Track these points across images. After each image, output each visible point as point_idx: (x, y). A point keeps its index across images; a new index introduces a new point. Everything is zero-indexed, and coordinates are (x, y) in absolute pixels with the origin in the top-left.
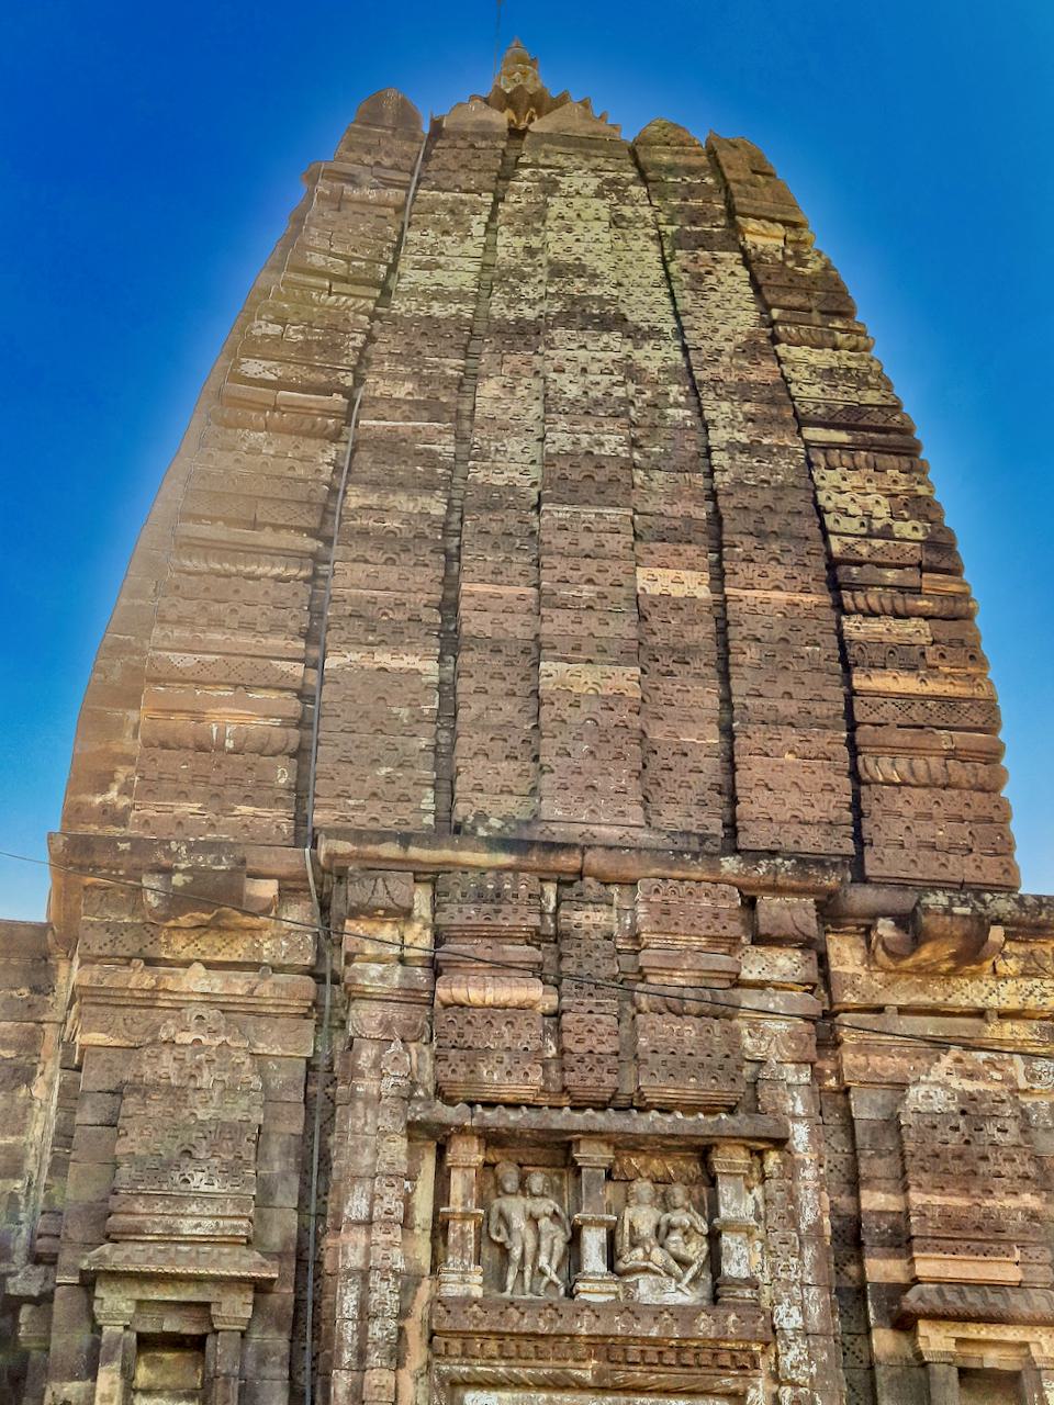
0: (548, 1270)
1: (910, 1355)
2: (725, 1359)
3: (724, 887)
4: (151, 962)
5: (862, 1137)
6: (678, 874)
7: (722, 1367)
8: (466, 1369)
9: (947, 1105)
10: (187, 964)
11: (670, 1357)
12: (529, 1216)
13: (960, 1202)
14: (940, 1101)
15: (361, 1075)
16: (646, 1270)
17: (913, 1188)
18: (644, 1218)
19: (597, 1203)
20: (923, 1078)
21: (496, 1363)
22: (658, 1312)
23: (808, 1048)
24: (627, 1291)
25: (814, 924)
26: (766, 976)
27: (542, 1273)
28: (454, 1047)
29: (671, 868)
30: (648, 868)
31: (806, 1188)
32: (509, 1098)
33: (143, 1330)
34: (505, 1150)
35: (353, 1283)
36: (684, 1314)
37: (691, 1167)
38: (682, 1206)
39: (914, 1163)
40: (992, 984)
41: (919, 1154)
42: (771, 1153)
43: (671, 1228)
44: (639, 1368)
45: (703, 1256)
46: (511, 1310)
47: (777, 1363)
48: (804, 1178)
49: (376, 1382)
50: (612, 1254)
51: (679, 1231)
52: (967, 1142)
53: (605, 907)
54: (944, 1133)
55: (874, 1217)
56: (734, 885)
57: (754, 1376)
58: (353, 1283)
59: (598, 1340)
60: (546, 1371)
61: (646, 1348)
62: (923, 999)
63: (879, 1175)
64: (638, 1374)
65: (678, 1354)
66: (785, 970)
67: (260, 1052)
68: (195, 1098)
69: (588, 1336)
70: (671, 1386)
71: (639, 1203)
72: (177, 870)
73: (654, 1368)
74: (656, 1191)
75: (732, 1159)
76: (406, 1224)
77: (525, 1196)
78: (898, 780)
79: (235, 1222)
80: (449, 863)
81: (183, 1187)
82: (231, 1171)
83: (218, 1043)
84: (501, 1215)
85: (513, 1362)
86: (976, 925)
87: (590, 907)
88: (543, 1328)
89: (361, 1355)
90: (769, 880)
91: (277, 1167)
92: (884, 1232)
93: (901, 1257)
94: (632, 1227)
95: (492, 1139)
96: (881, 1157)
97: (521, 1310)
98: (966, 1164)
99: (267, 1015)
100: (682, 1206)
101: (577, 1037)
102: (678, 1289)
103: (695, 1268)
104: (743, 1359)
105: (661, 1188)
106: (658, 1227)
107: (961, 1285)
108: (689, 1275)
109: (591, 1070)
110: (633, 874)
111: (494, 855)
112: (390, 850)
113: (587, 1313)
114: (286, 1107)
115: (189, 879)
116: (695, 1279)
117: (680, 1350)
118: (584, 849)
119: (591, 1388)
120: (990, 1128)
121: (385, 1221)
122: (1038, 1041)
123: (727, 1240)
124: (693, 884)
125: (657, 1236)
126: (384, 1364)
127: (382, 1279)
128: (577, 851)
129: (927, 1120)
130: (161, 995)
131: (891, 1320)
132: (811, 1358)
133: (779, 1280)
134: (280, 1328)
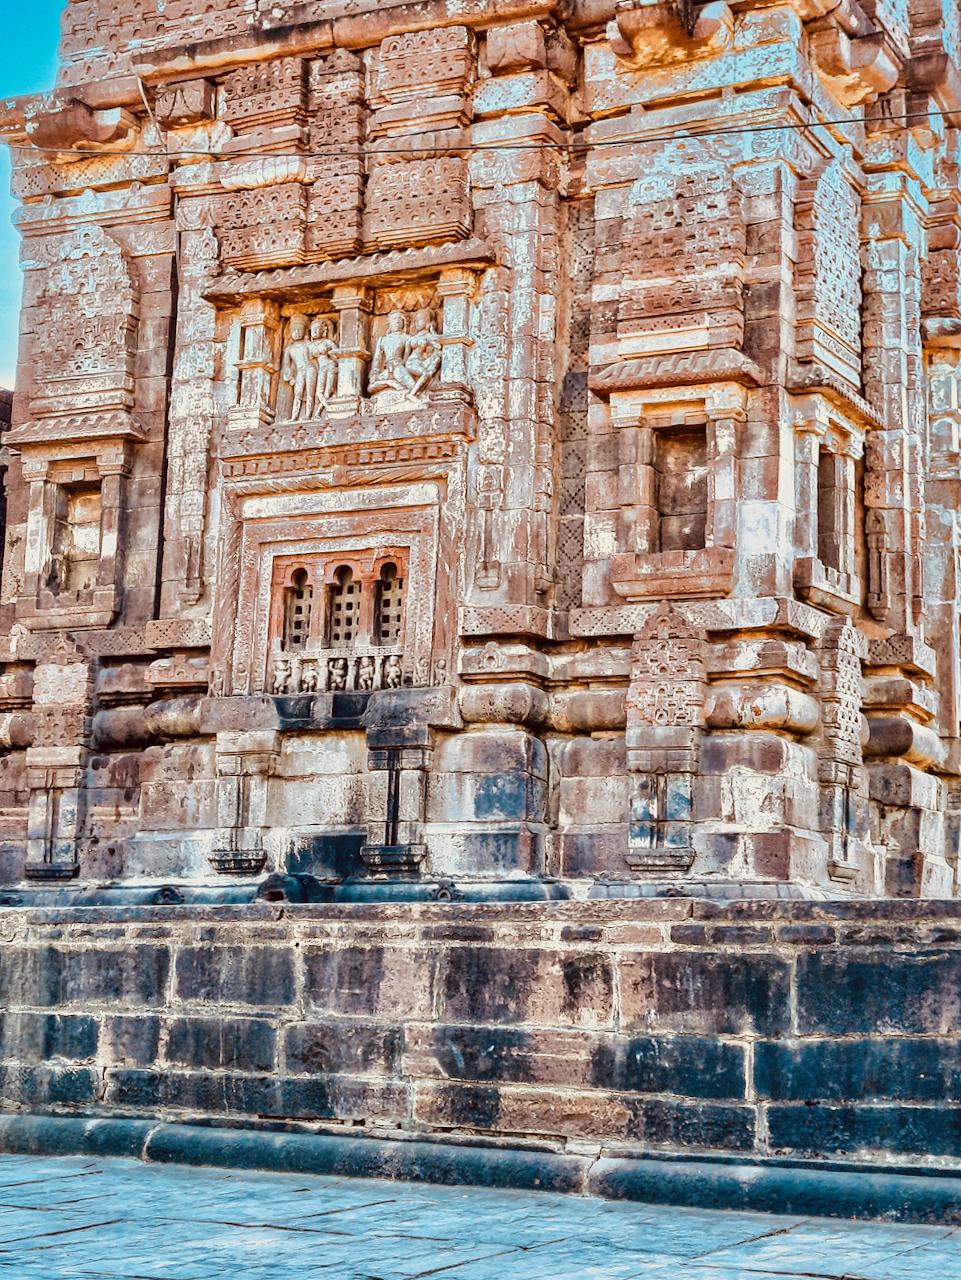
3: (454, 29)
4: (59, 195)
6: (413, 26)
10: (79, 193)
13: (665, 282)
26: (502, 106)
29: (405, 23)
30: (387, 26)
32: (281, 262)
40: (730, 60)
62: (667, 91)
68: (82, 302)
72: (27, 120)
79: (113, 394)
80: (227, 64)
81: (76, 372)
82: (108, 355)
87: (339, 76)
88: (294, 446)
90: (490, 12)
91: (152, 345)
95: (278, 299)
99: (144, 221)
104: (446, 449)
111: (261, 47)
112: (182, 63)
114: (158, 296)
115: (36, 125)
117: (398, 449)
118: (331, 23)
120: (700, 207)
128: (327, 26)
130: (67, 221)
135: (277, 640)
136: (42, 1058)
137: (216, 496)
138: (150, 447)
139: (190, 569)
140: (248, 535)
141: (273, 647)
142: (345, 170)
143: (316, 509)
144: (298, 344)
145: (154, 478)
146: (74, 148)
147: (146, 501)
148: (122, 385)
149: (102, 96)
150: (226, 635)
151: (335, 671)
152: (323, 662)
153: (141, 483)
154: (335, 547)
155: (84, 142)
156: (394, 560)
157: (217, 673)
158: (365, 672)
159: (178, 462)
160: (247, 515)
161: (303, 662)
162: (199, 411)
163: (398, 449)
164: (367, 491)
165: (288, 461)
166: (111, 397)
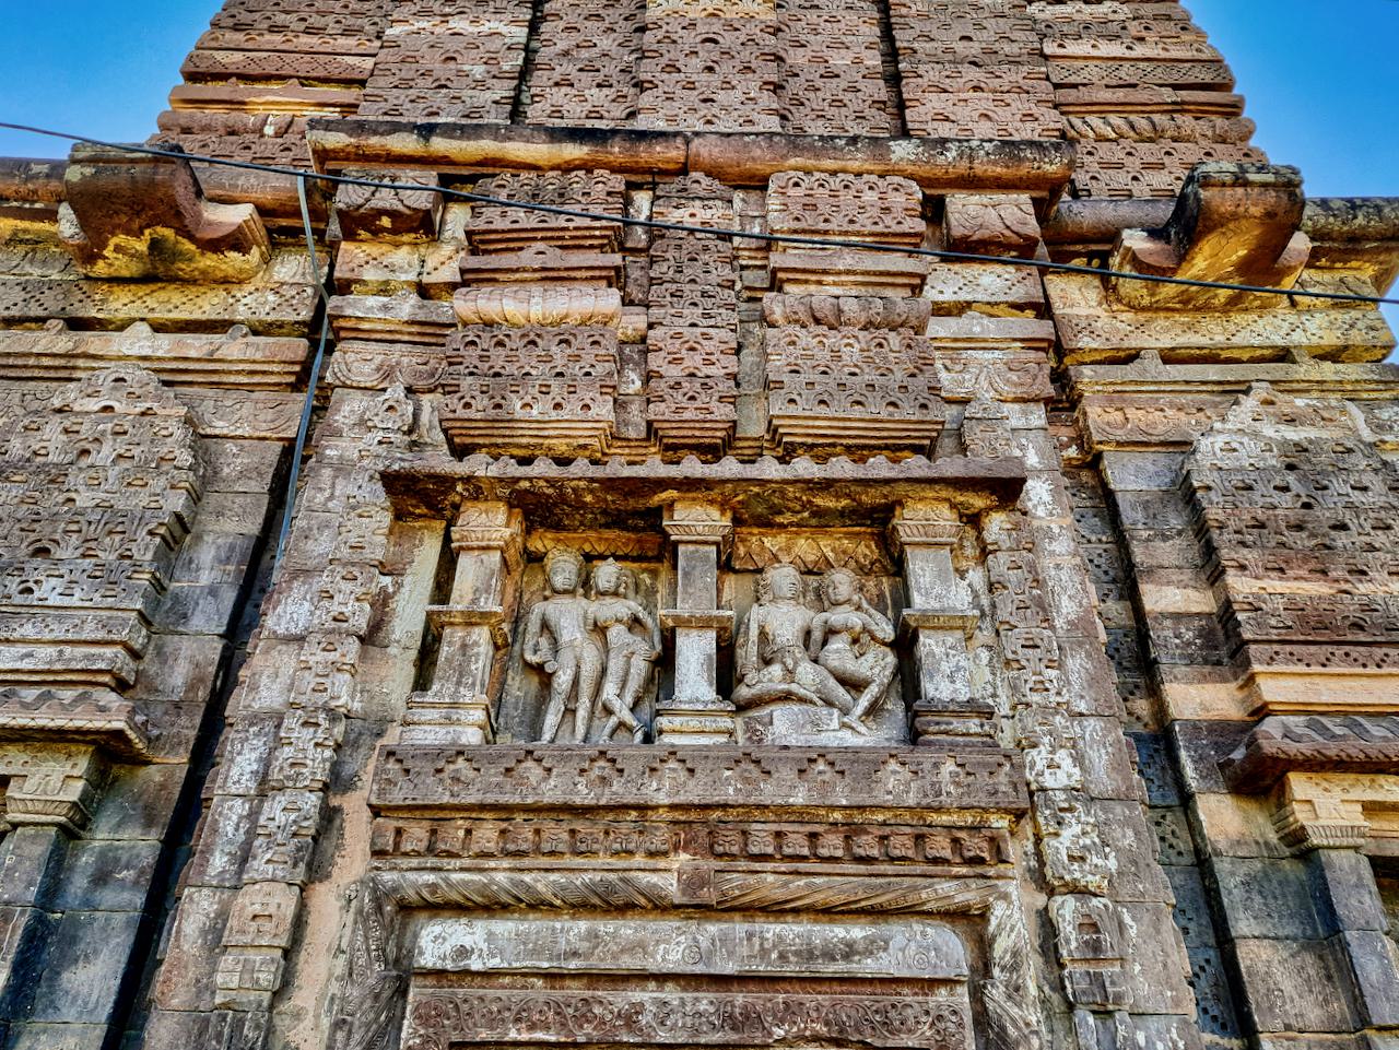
0: (616, 704)
1: (1273, 838)
2: (940, 846)
3: (897, 179)
5: (1130, 515)
6: (829, 164)
7: (936, 861)
8: (431, 878)
9: (1264, 459)
11: (832, 844)
12: (588, 624)
14: (1249, 453)
15: (338, 434)
16: (787, 697)
17: (1231, 572)
18: (785, 620)
19: (696, 592)
20: (1218, 425)
21: (492, 864)
22: (807, 761)
23: (1038, 381)
24: (748, 728)
25: (1033, 221)
26: (964, 296)
27: (609, 712)
28: (471, 374)
29: (817, 157)
30: (784, 157)
31: (1058, 566)
34: (562, 536)
35: (256, 735)
36: (864, 764)
37: (862, 549)
38: (849, 601)
39: (1226, 537)
41: (1232, 524)
42: (994, 515)
43: (830, 632)
44: (769, 866)
45: (888, 672)
46: (530, 764)
47: (1039, 854)
48: (1052, 553)
49: (257, 909)
50: (726, 675)
51: (846, 637)
52: (1307, 506)
53: (719, 203)
54: (1263, 494)
55: (1168, 623)
56: (911, 177)
57: (999, 877)
58: (256, 735)
59: (693, 816)
60: (587, 877)
61: (785, 827)
63: (1166, 563)
64: (771, 878)
65: (847, 838)
66: (993, 289)
67: (217, 432)
68: (75, 479)
69: (673, 807)
70: (836, 899)
71: (773, 600)
73: (802, 866)
74: (806, 584)
75: (925, 518)
76: (372, 637)
77: (586, 595)
78: (1114, 135)
80: (484, 162)
81: (19, 599)
82: (104, 577)
83: (138, 410)
84: (545, 626)
85: (526, 862)
86: (1285, 197)
87: (698, 203)
88: (584, 795)
89: (244, 857)
90: (963, 167)
91: (205, 578)
92: (1189, 644)
93: (1224, 680)
94: (763, 634)
95: (539, 510)
96: (1165, 538)
97: (546, 764)
98: (1313, 535)
100: (849, 601)
101: (670, 357)
102: (844, 725)
103: (873, 690)
104: (976, 845)
105: (813, 581)
106: (808, 633)
107: (1347, 713)
108: (864, 701)
109: (692, 398)
110: (761, 168)
113: (672, 764)
114: (240, 500)
116: (874, 710)
119: (677, 907)
120: (1338, 485)
121: (332, 632)
122: (1377, 382)
123: (928, 644)
124: (851, 177)
125: (807, 647)
126: (280, 874)
127: (306, 724)
129: (1236, 479)
130: (80, 363)
131: (1228, 779)
132: (1105, 844)
133: (1028, 705)
134: (149, 822)
136: (183, 73)
137: (328, 904)
138: (153, 774)
140: (422, 1019)
142: (712, 322)
143: (628, 963)
144: (566, 601)
145: (143, 844)
146: (141, 246)
147: (108, 897)
148: (124, 635)
149: (222, 187)
153: (103, 854)
155: (168, 233)
162: (321, 698)
163: (851, 831)
164: (772, 929)
165: (556, 833)
166: (87, 657)
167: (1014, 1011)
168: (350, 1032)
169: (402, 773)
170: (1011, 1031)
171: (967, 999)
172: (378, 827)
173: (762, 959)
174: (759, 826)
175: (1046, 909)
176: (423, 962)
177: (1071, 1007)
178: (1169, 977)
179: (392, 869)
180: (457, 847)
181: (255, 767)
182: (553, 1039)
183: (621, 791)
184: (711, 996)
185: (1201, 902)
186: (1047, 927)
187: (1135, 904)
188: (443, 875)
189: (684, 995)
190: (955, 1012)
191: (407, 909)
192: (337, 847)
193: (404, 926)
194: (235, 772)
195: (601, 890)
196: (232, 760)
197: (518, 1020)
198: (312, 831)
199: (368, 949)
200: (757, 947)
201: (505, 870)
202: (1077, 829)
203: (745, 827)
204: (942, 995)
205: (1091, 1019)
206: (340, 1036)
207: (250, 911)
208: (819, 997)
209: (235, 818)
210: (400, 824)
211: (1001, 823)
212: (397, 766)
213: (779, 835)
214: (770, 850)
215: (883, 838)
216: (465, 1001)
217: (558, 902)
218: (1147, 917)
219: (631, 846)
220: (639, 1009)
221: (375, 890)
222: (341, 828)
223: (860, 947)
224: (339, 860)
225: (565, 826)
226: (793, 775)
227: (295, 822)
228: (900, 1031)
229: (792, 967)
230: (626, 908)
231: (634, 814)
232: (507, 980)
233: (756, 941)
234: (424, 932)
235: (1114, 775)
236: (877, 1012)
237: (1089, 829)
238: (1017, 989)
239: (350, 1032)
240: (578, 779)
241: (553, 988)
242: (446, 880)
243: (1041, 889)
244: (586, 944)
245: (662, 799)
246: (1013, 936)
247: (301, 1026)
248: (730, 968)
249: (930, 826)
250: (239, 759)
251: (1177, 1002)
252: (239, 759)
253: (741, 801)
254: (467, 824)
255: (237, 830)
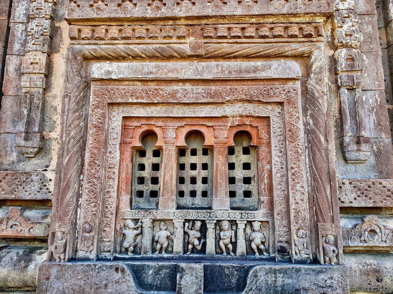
2: (294, 30)
8: (94, 47)
11: (251, 31)
21: (117, 42)
33: (178, 145)
44: (225, 41)
49: (32, 61)
59: (195, 22)
61: (232, 26)
65: (257, 29)
69: (187, 18)
85: (130, 41)
88: (150, 13)
104: (309, 29)
126: (38, 48)
135: (125, 198)
137: (60, 62)
139: (29, 123)
141: (122, 205)
143: (172, 75)
150: (70, 194)
151: (191, 233)
152: (178, 223)
154: (188, 112)
156: (248, 129)
157: (59, 235)
158: (227, 234)
159: (21, 27)
160: (96, 75)
161: (154, 221)
163: (259, 25)
164: (226, 64)
167: (318, 87)
168: (70, 98)
169: (77, 7)
170: (316, 94)
171: (300, 85)
172: (71, 27)
173: (222, 73)
174: (221, 26)
175: (333, 55)
176: (94, 76)
177: (339, 88)
178: (378, 77)
179: (79, 44)
180: (102, 36)
181: (24, 12)
182: (145, 102)
183: (165, 12)
184: (203, 87)
185: (386, 61)
186: (334, 61)
187: (370, 52)
188: (98, 46)
189: (193, 87)
190: (295, 90)
191: (86, 59)
192: (60, 41)
193: (87, 66)
194: (17, 14)
195: (159, 50)
196: (15, 9)
197: (132, 96)
198: (49, 34)
199: (73, 71)
200: (220, 70)
201: (122, 44)
202: (350, 24)
203: (216, 26)
204: (290, 84)
205: (346, 91)
206: (66, 100)
207: (29, 61)
208: (243, 87)
209: (20, 31)
210: (79, 27)
211: (320, 20)
212: (75, 4)
213: (229, 29)
214: (226, 34)
215: (272, 29)
216: (112, 90)
217: (144, 56)
218: (372, 57)
219: (171, 34)
220: (176, 92)
221: (73, 52)
222: (61, 34)
223: (260, 68)
224: (62, 46)
225: (144, 27)
226: (236, 3)
227: (41, 30)
228: (273, 97)
229: (233, 76)
230: (170, 58)
231: (171, 22)
232: (127, 83)
233: (220, 67)
234: (93, 66)
235: (367, 5)
236: (265, 91)
237: (355, 24)
238: (320, 80)
239: (70, 98)
240: (147, 7)
241: (144, 85)
242: (100, 48)
243: (332, 49)
244: (155, 70)
245: (182, 14)
246: (321, 62)
247: (56, 100)
248: (210, 77)
249: (291, 23)
250: (17, 9)
251: (379, 86)
252: (17, 9)
253: (214, 14)
254: (106, 27)
255: (22, 35)
